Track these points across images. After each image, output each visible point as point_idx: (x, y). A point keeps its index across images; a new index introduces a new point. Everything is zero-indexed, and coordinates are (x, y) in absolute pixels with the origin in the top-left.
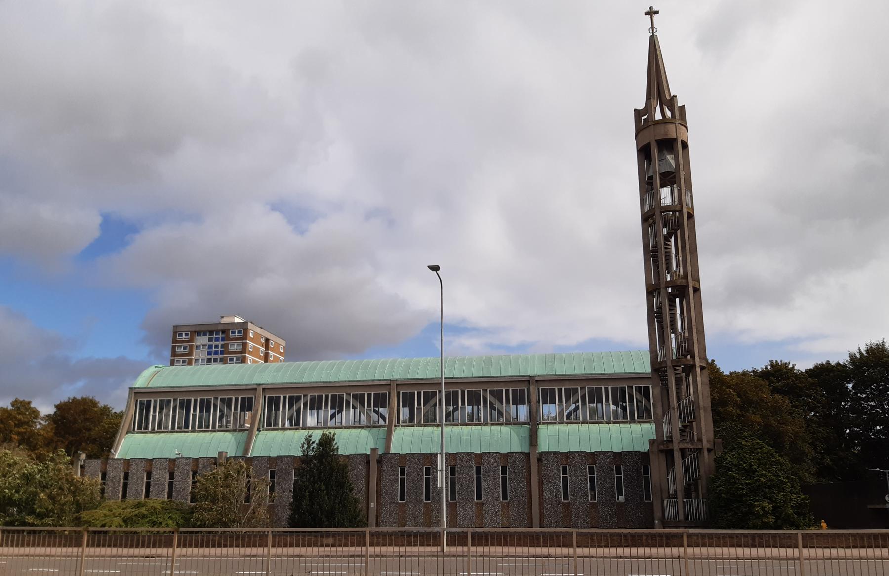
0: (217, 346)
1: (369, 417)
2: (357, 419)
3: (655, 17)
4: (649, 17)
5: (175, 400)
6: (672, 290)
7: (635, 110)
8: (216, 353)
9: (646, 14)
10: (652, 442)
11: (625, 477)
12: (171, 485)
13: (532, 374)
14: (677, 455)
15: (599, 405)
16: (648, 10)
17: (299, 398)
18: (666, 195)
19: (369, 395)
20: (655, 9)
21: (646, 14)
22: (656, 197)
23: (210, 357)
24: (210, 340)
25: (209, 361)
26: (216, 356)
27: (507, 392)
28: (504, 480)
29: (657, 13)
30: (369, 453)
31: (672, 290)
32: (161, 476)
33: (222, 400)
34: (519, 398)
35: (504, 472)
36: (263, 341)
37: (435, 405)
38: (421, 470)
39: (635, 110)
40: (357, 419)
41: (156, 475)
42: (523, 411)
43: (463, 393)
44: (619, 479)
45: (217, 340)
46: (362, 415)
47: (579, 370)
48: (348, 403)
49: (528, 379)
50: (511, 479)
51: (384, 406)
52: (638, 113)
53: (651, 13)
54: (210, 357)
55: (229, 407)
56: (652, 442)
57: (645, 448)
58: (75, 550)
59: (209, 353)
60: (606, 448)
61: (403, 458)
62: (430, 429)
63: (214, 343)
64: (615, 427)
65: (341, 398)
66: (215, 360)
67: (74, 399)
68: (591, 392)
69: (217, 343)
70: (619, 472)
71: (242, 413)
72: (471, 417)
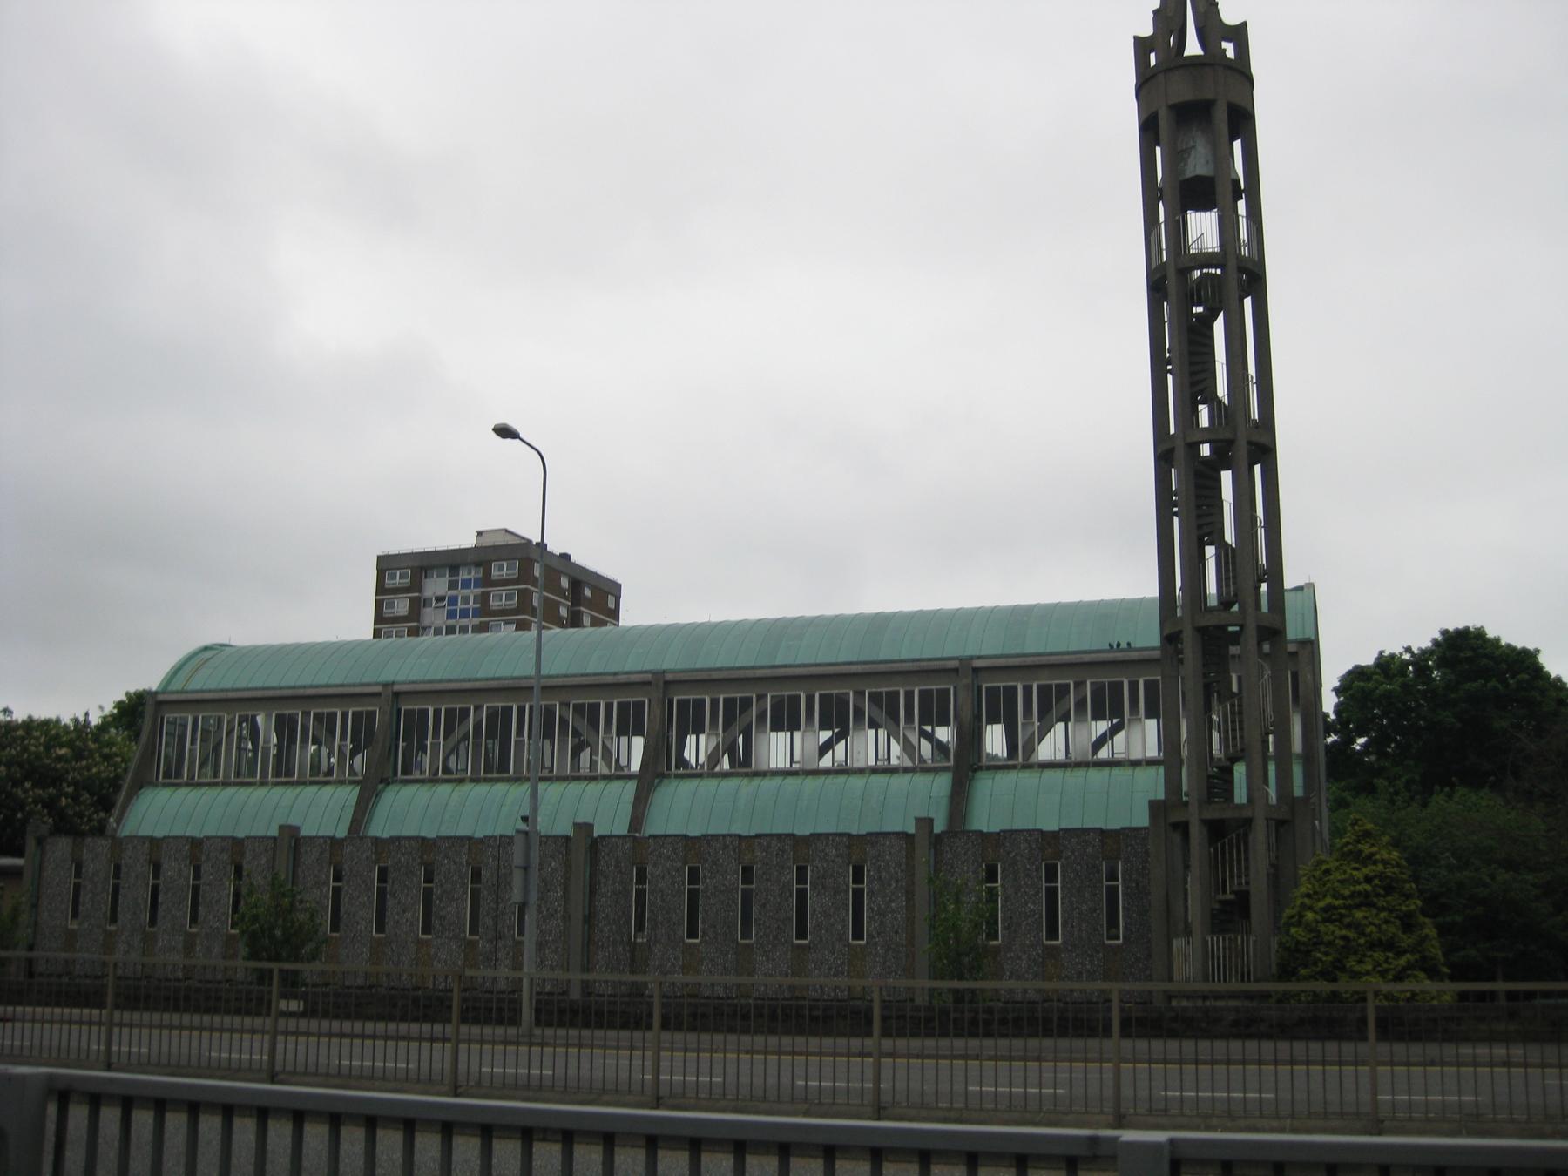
0: (466, 600)
1: (908, 748)
6: (1213, 448)
7: (1136, 38)
8: (465, 614)
10: (1154, 806)
11: (1126, 887)
12: (196, 889)
14: (1196, 831)
15: (547, 742)
18: (1203, 229)
19: (609, 707)
22: (1178, 231)
23: (451, 622)
26: (464, 622)
27: (909, 695)
31: (1213, 448)
32: (175, 870)
34: (630, 723)
35: (858, 878)
36: (565, 583)
38: (680, 871)
39: (1136, 38)
41: (169, 869)
42: (635, 751)
45: (466, 584)
48: (859, 713)
49: (955, 664)
50: (871, 893)
51: (944, 722)
52: (1142, 46)
54: (451, 622)
55: (594, 724)
56: (1154, 806)
57: (1142, 819)
58: (96, 1012)
59: (451, 615)
62: (500, 788)
63: (461, 592)
66: (464, 630)
67: (1467, 630)
68: (1098, 692)
69: (466, 592)
70: (1112, 876)
71: (624, 740)
72: (316, 768)
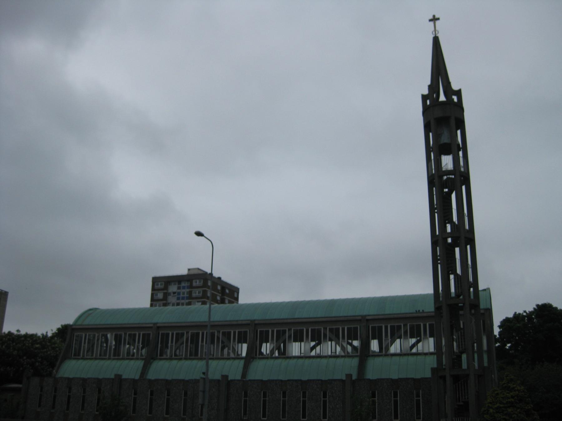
0: (184, 293)
2: (333, 350)
3: (437, 22)
4: (432, 23)
5: (290, 330)
8: (183, 298)
9: (430, 20)
13: (365, 313)
16: (431, 17)
17: (284, 332)
18: (447, 162)
20: (437, 17)
21: (430, 20)
24: (179, 288)
25: (178, 304)
26: (183, 301)
28: (325, 402)
29: (438, 19)
30: (344, 378)
31: (452, 239)
33: (331, 330)
35: (325, 396)
36: (219, 288)
37: (183, 343)
40: (333, 350)
42: (244, 349)
43: (386, 328)
44: (418, 401)
45: (184, 288)
46: (337, 346)
47: (284, 315)
49: (360, 318)
52: (424, 98)
53: (434, 19)
57: (428, 374)
60: (78, 376)
61: (263, 384)
62: (195, 362)
63: (182, 291)
64: (188, 362)
65: (319, 331)
66: (183, 304)
68: (412, 328)
69: (184, 290)
70: (418, 396)
71: (240, 345)
72: (128, 353)
